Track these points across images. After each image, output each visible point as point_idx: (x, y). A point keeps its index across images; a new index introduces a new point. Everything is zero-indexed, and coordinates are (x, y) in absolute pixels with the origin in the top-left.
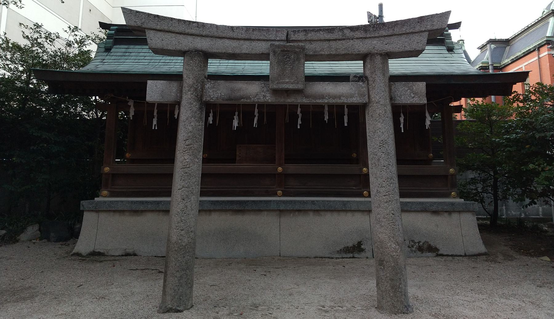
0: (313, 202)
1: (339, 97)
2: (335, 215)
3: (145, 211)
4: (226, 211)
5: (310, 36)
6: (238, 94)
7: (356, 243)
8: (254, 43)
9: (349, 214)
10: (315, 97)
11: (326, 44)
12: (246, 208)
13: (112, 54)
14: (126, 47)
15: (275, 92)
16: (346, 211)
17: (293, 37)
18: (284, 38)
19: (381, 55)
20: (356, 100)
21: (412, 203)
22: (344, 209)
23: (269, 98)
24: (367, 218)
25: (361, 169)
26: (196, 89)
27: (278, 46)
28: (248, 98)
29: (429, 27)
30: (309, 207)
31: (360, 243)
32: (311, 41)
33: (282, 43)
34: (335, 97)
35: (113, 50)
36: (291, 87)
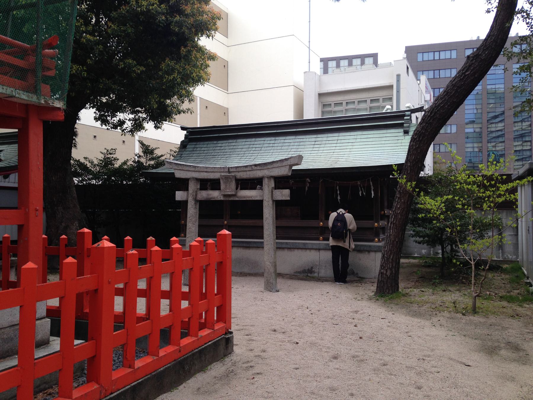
0: (287, 243)
1: (251, 197)
2: (300, 251)
3: (286, 248)
4: (240, 247)
5: (238, 169)
6: (211, 196)
7: (310, 268)
8: (215, 173)
9: (308, 251)
10: (241, 197)
11: (245, 173)
12: (251, 246)
13: (187, 150)
14: (195, 143)
15: (225, 196)
16: (306, 249)
17: (231, 170)
18: (227, 171)
19: (268, 178)
20: (258, 198)
21: (365, 245)
22: (305, 248)
23: (222, 198)
24: (318, 253)
25: (319, 223)
26: (193, 195)
27: (224, 176)
28: (214, 198)
29: (289, 164)
30: (284, 246)
31: (312, 268)
32: (238, 172)
33: (225, 174)
34: (249, 197)
35: (188, 147)
36: (229, 193)
